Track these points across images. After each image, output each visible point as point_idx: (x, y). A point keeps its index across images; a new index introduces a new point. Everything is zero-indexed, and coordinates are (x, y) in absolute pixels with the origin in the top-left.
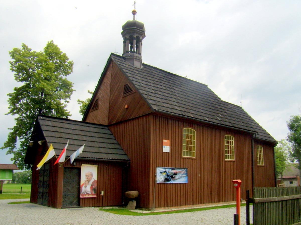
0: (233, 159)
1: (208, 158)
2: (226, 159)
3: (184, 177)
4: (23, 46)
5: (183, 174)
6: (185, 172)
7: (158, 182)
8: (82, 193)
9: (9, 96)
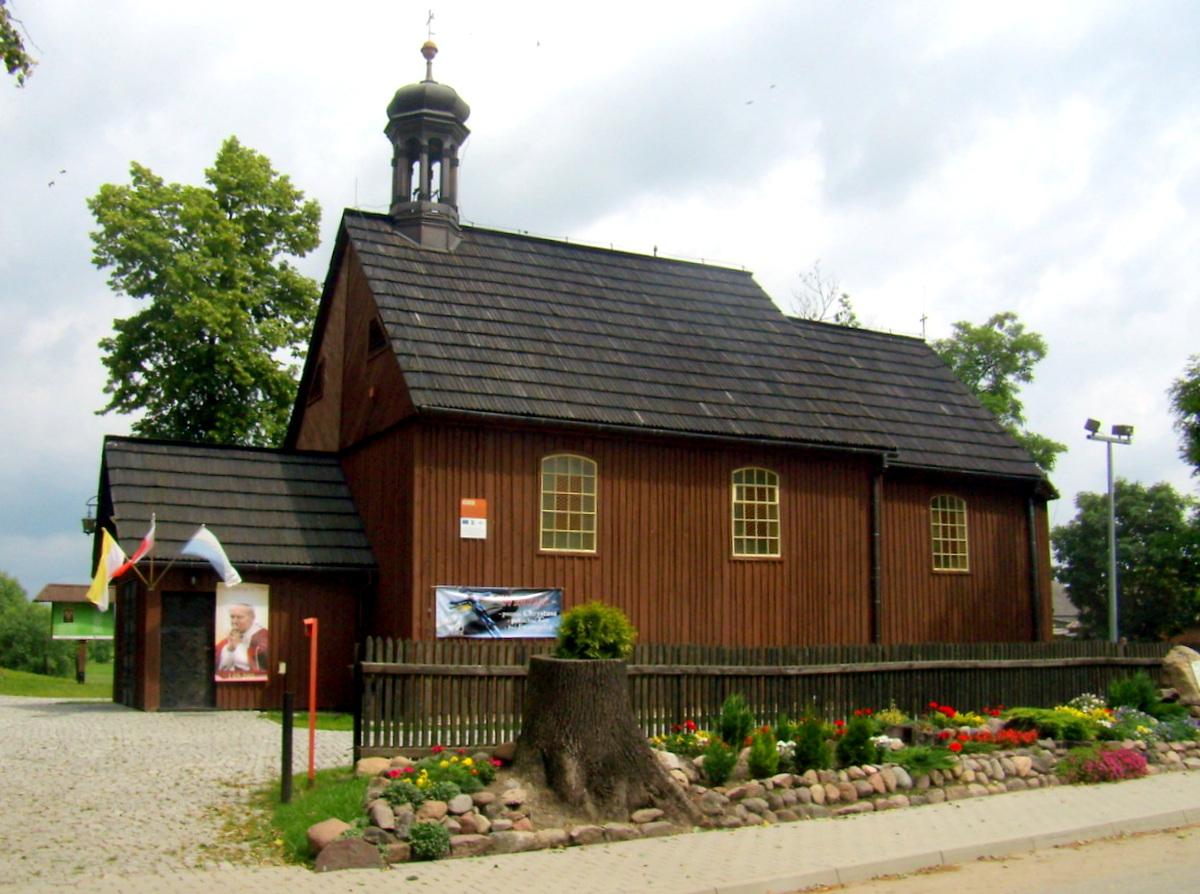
0: (774, 550)
1: (654, 553)
2: (736, 555)
3: (546, 617)
4: (133, 173)
5: (542, 609)
6: (549, 601)
7: (441, 633)
8: (220, 667)
9: (102, 350)
